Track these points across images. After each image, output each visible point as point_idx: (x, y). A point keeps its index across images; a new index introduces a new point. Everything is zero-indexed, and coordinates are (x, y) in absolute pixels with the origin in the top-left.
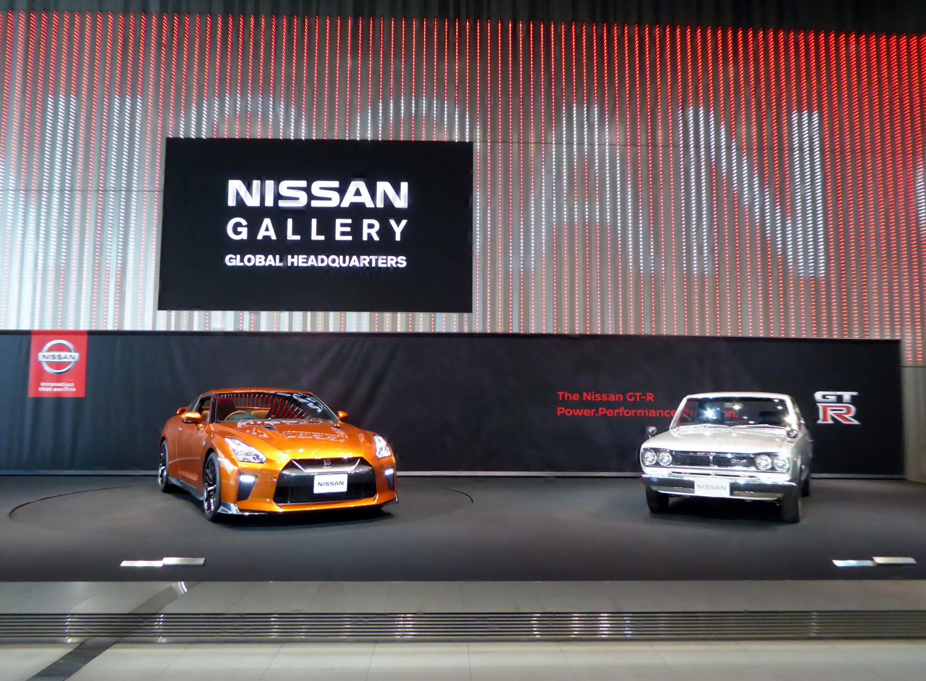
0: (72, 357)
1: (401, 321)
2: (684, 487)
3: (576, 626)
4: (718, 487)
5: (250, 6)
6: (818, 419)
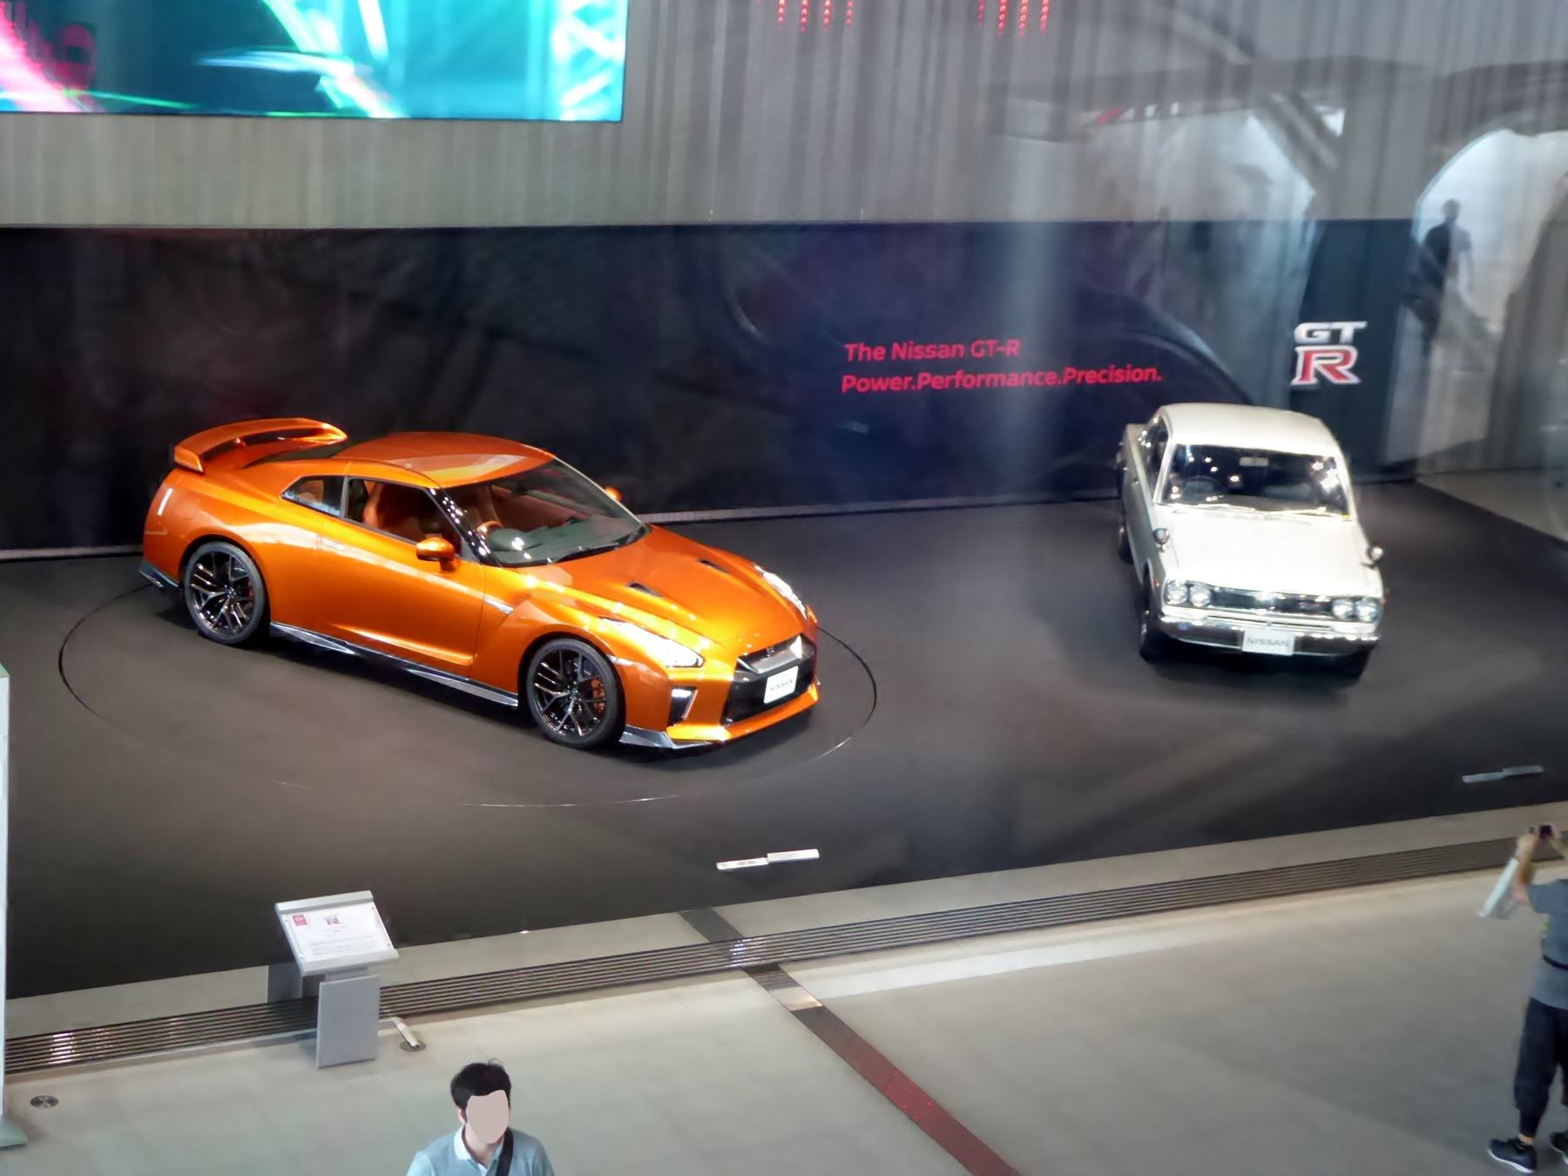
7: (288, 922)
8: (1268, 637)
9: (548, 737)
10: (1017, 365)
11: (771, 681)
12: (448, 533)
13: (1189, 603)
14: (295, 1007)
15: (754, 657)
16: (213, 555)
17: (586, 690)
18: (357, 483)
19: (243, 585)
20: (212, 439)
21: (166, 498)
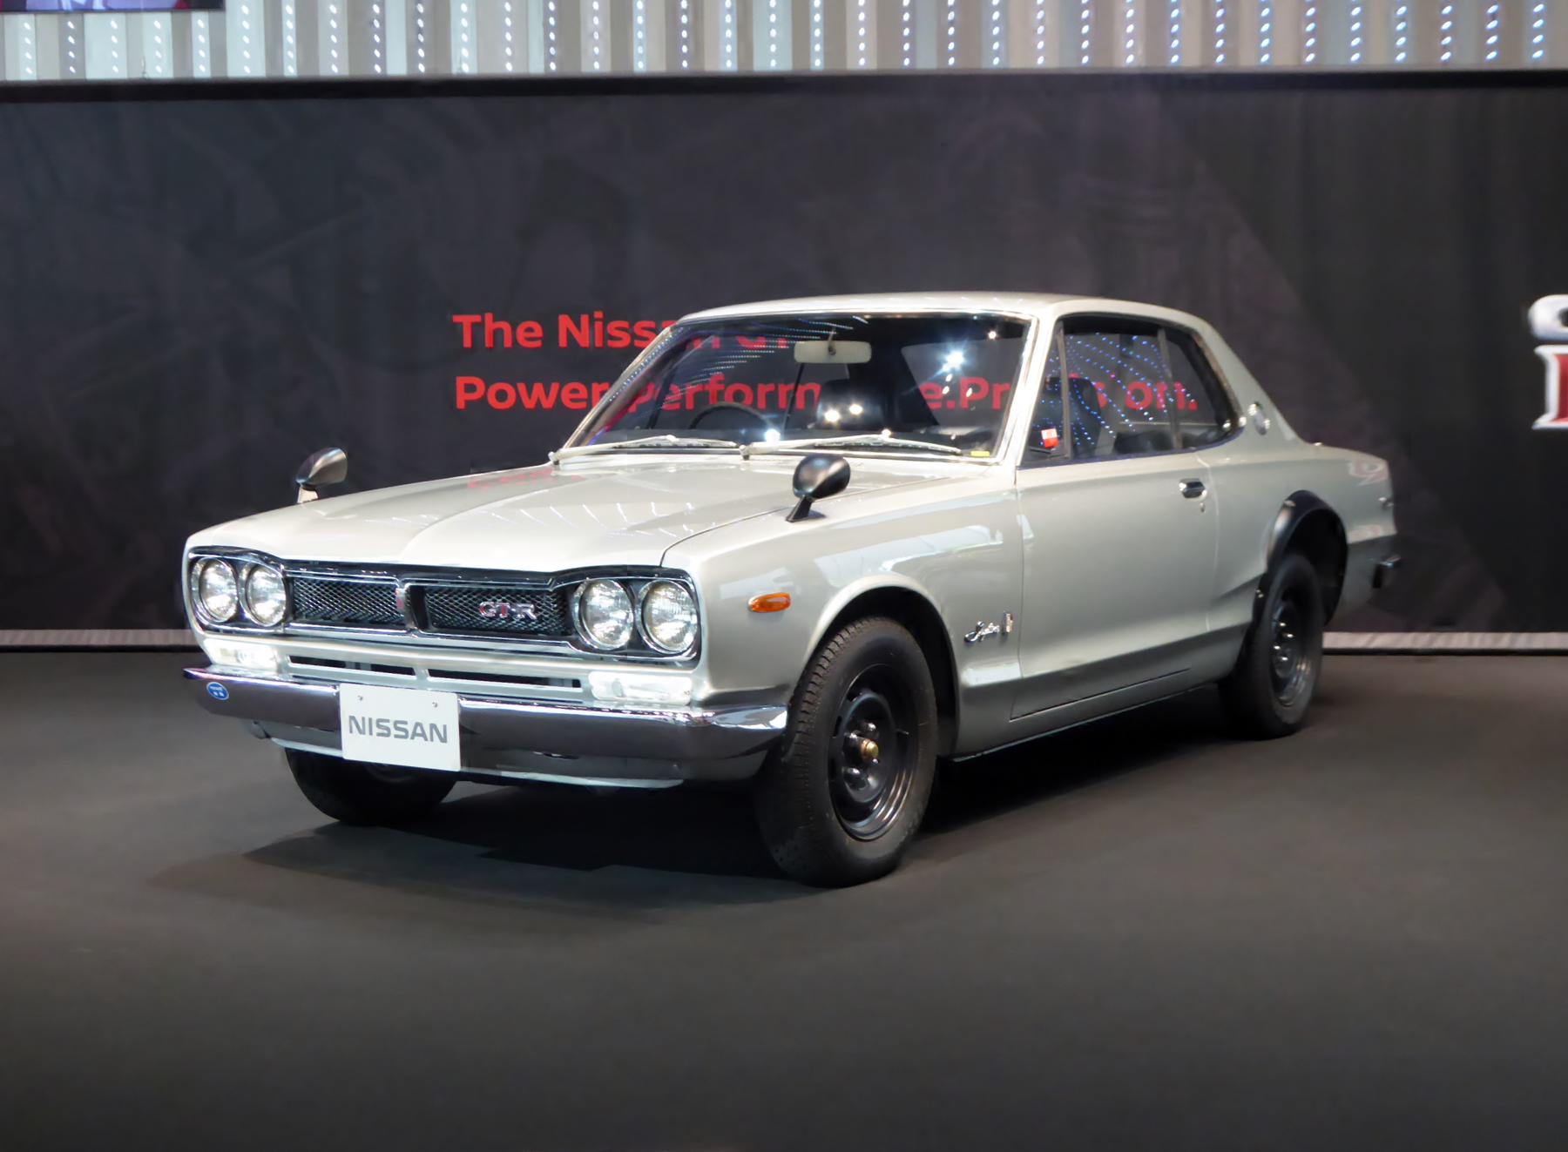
1: (647, 13)
2: (309, 723)
4: (418, 732)
6: (1541, 410)
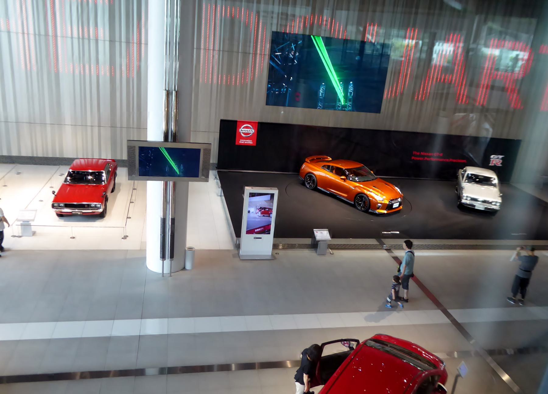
0: (252, 131)
2: (166, 210)
3: (469, 199)
5: (271, 2)
7: (315, 232)
8: (479, 206)
9: (358, 209)
10: (435, 155)
11: (394, 204)
12: (346, 176)
13: (466, 200)
14: (315, 245)
15: (392, 200)
16: (310, 176)
17: (364, 202)
18: (332, 166)
19: (314, 181)
20: (311, 158)
21: (304, 166)
